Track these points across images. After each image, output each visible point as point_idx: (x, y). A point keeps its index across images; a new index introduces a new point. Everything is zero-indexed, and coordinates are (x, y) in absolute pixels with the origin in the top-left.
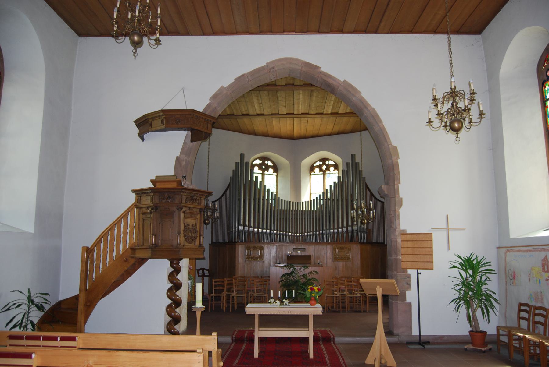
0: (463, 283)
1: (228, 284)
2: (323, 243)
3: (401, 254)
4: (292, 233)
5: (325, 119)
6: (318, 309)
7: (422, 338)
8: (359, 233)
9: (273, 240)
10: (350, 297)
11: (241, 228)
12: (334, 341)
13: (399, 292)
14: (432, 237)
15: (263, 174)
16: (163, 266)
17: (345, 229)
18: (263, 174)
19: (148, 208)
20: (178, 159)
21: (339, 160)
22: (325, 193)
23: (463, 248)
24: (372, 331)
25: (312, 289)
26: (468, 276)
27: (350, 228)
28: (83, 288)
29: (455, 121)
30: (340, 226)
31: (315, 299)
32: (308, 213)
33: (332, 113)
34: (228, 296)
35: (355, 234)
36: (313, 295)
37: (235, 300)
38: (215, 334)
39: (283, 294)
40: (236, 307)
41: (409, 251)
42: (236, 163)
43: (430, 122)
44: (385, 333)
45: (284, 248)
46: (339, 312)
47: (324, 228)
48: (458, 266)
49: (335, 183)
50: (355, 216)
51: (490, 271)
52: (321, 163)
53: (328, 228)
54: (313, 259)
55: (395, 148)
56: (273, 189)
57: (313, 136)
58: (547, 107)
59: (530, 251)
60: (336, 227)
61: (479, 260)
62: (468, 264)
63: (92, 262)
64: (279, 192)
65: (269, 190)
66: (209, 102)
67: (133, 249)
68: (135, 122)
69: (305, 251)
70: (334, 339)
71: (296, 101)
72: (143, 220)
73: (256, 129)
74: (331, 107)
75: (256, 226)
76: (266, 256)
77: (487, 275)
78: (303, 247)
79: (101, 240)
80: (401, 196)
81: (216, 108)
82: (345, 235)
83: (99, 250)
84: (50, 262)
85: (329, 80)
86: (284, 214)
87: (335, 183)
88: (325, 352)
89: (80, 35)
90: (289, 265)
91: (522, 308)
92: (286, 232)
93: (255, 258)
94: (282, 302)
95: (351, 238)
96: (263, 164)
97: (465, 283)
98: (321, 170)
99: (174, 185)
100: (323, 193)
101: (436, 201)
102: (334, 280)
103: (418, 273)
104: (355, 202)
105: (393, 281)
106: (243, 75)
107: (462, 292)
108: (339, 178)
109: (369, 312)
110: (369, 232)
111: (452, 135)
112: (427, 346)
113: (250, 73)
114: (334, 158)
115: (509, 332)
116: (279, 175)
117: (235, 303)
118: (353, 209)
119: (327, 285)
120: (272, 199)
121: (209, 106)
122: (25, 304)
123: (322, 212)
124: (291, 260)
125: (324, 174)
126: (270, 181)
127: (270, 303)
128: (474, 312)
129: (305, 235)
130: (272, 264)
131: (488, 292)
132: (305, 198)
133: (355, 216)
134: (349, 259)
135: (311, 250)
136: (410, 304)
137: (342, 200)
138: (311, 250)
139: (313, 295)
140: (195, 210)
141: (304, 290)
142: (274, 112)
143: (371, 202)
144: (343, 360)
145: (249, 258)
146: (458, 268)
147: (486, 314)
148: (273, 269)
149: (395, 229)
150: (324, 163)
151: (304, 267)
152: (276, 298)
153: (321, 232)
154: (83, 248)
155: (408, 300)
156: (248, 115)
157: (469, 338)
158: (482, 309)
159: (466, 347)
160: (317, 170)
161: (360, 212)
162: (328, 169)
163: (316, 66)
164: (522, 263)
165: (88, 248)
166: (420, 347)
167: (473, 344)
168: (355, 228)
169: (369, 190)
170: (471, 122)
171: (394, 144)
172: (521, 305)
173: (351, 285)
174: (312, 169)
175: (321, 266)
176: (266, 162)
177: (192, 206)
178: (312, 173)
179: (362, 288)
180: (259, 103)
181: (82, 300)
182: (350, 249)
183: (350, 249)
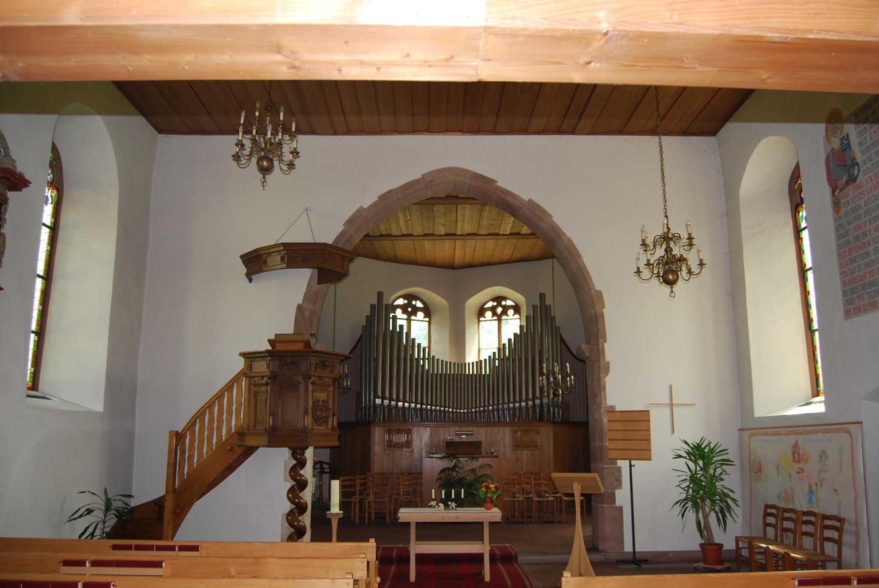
0: (692, 477)
1: (361, 485)
2: (499, 423)
3: (608, 440)
4: (453, 408)
5: (501, 242)
6: (496, 514)
7: (637, 555)
8: (551, 409)
9: (424, 418)
10: (538, 502)
11: (378, 401)
12: (516, 561)
13: (603, 490)
14: (649, 415)
15: (409, 320)
16: (282, 456)
17: (530, 403)
18: (409, 320)
19: (262, 377)
20: (299, 307)
21: (521, 299)
22: (502, 348)
23: (692, 427)
24: (568, 546)
25: (487, 487)
26: (698, 469)
27: (538, 402)
28: (171, 488)
29: (669, 271)
30: (524, 398)
31: (492, 501)
32: (478, 378)
33: (511, 234)
34: (361, 501)
35: (545, 409)
36: (489, 495)
37: (373, 507)
38: (372, 540)
39: (448, 494)
40: (373, 517)
41: (619, 435)
42: (371, 305)
43: (638, 272)
44: (587, 549)
45: (442, 430)
46: (522, 523)
47: (501, 401)
48: (685, 455)
49: (515, 334)
50: (545, 385)
51: (726, 462)
52: (495, 304)
53: (506, 400)
54: (484, 446)
55: (600, 293)
56: (424, 344)
57: (483, 265)
58: (802, 239)
59: (779, 434)
60: (518, 399)
61: (712, 446)
62: (699, 453)
63: (183, 453)
64: (432, 347)
65: (419, 345)
66: (342, 228)
67: (241, 434)
68: (243, 257)
69: (472, 435)
70: (516, 557)
71: (459, 218)
72: (256, 394)
73: (399, 254)
74: (510, 226)
75: (401, 398)
76: (416, 443)
77: (724, 467)
78: (470, 429)
79: (195, 421)
80: (607, 360)
81: (351, 237)
82: (531, 411)
83: (193, 435)
84: (120, 451)
85: (510, 199)
86: (441, 380)
87: (515, 334)
88: (505, 574)
89: (160, 131)
90: (449, 456)
91: (769, 511)
92: (445, 407)
93: (399, 446)
94: (447, 506)
95: (540, 416)
96: (409, 304)
97: (693, 479)
98: (494, 314)
99: (300, 347)
100: (499, 349)
101: (657, 366)
102: (515, 477)
103: (631, 466)
104: (545, 365)
105: (596, 475)
106: (390, 192)
107: (691, 491)
108: (521, 327)
109: (566, 523)
110: (565, 406)
111: (666, 289)
112: (644, 566)
113: (400, 188)
114: (513, 297)
115: (750, 543)
116: (432, 321)
117: (373, 511)
118: (542, 374)
119: (506, 483)
120: (424, 359)
121: (342, 233)
122: (100, 509)
123: (498, 376)
124: (452, 449)
125: (500, 320)
126: (419, 330)
127: (430, 507)
128: (706, 517)
129: (472, 412)
130: (424, 454)
131: (725, 491)
132: (471, 357)
133: (545, 385)
134: (536, 446)
135: (481, 434)
136: (620, 509)
137: (526, 360)
138: (481, 434)
139: (489, 495)
140: (326, 380)
141: (478, 489)
142: (427, 232)
143: (568, 365)
144: (530, 583)
145: (390, 445)
146: (685, 458)
147: (723, 521)
148: (427, 462)
149: (600, 405)
150: (499, 304)
151: (472, 458)
152: (439, 500)
153: (495, 407)
154: (170, 432)
155: (618, 504)
156: (390, 235)
157: (701, 555)
158: (716, 513)
159: (695, 565)
160: (488, 314)
161: (552, 379)
162: (505, 312)
163: (491, 179)
164: (771, 451)
165: (177, 432)
166: (635, 566)
167: (705, 561)
168: (545, 401)
169: (565, 344)
170: (690, 272)
171: (598, 287)
172: (767, 507)
173: (540, 484)
174: (481, 312)
175: (497, 457)
176: (414, 302)
177: (323, 375)
178: (482, 319)
179: (555, 489)
180: (406, 221)
181: (169, 505)
182: (538, 432)
183: (538, 432)
